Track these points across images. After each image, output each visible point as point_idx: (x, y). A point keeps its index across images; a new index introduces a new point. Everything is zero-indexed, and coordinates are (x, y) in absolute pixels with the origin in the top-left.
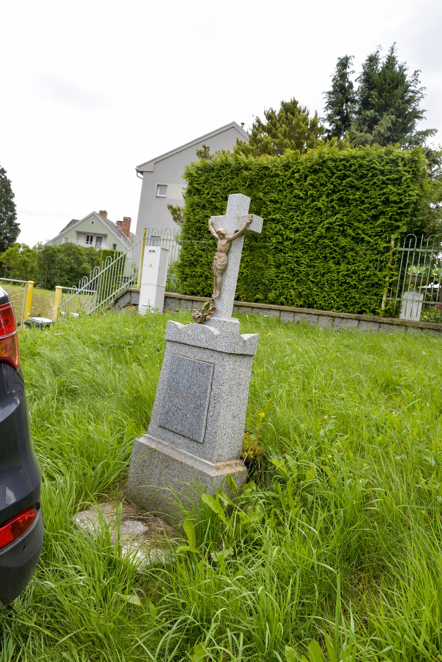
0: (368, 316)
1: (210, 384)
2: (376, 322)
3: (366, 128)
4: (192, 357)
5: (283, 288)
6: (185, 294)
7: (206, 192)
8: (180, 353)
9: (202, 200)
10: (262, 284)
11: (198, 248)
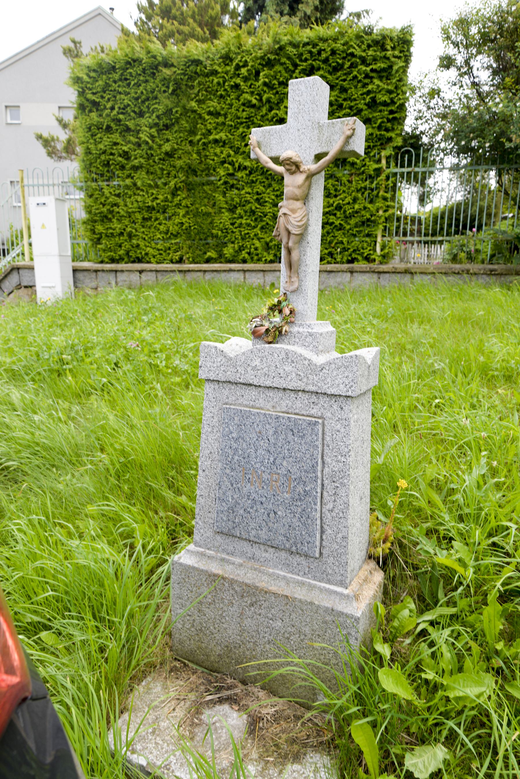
0: (361, 265)
1: (320, 456)
2: (374, 272)
3: (287, 8)
4: (269, 406)
5: (243, 239)
6: (102, 262)
7: (109, 105)
8: (239, 402)
9: (104, 119)
10: (213, 237)
11: (110, 193)
